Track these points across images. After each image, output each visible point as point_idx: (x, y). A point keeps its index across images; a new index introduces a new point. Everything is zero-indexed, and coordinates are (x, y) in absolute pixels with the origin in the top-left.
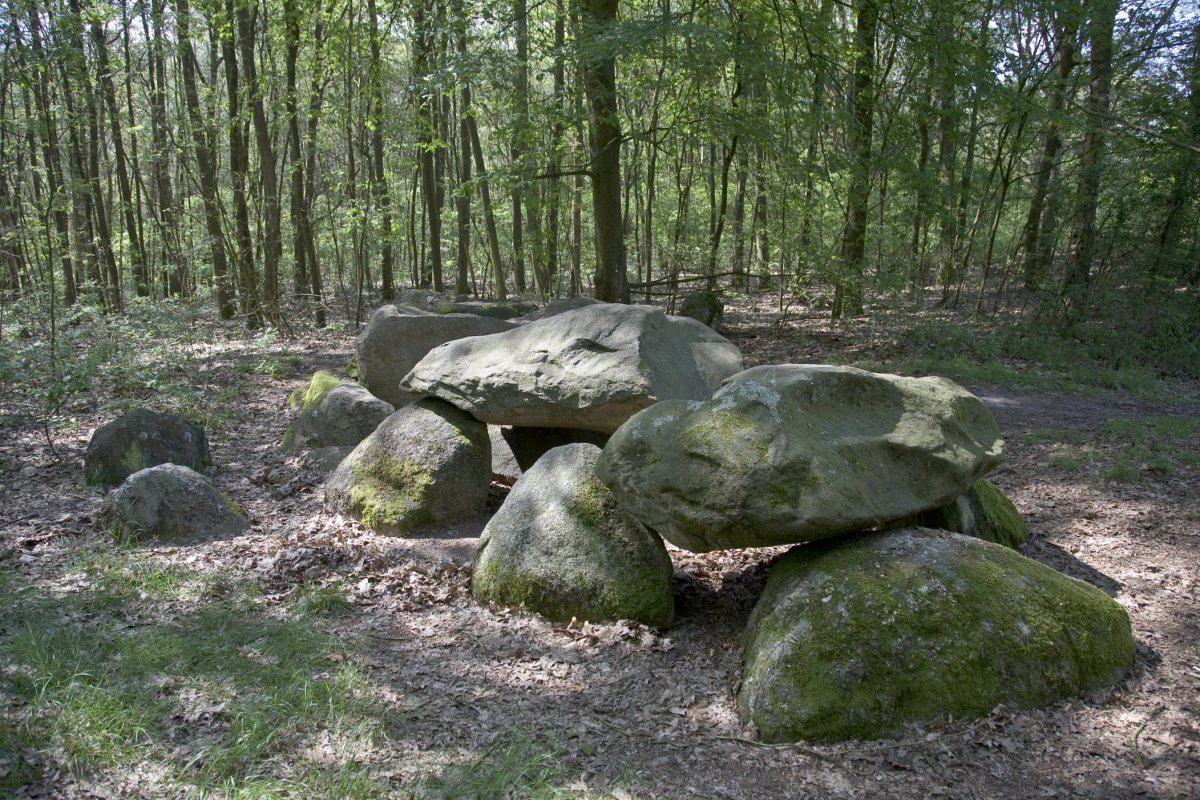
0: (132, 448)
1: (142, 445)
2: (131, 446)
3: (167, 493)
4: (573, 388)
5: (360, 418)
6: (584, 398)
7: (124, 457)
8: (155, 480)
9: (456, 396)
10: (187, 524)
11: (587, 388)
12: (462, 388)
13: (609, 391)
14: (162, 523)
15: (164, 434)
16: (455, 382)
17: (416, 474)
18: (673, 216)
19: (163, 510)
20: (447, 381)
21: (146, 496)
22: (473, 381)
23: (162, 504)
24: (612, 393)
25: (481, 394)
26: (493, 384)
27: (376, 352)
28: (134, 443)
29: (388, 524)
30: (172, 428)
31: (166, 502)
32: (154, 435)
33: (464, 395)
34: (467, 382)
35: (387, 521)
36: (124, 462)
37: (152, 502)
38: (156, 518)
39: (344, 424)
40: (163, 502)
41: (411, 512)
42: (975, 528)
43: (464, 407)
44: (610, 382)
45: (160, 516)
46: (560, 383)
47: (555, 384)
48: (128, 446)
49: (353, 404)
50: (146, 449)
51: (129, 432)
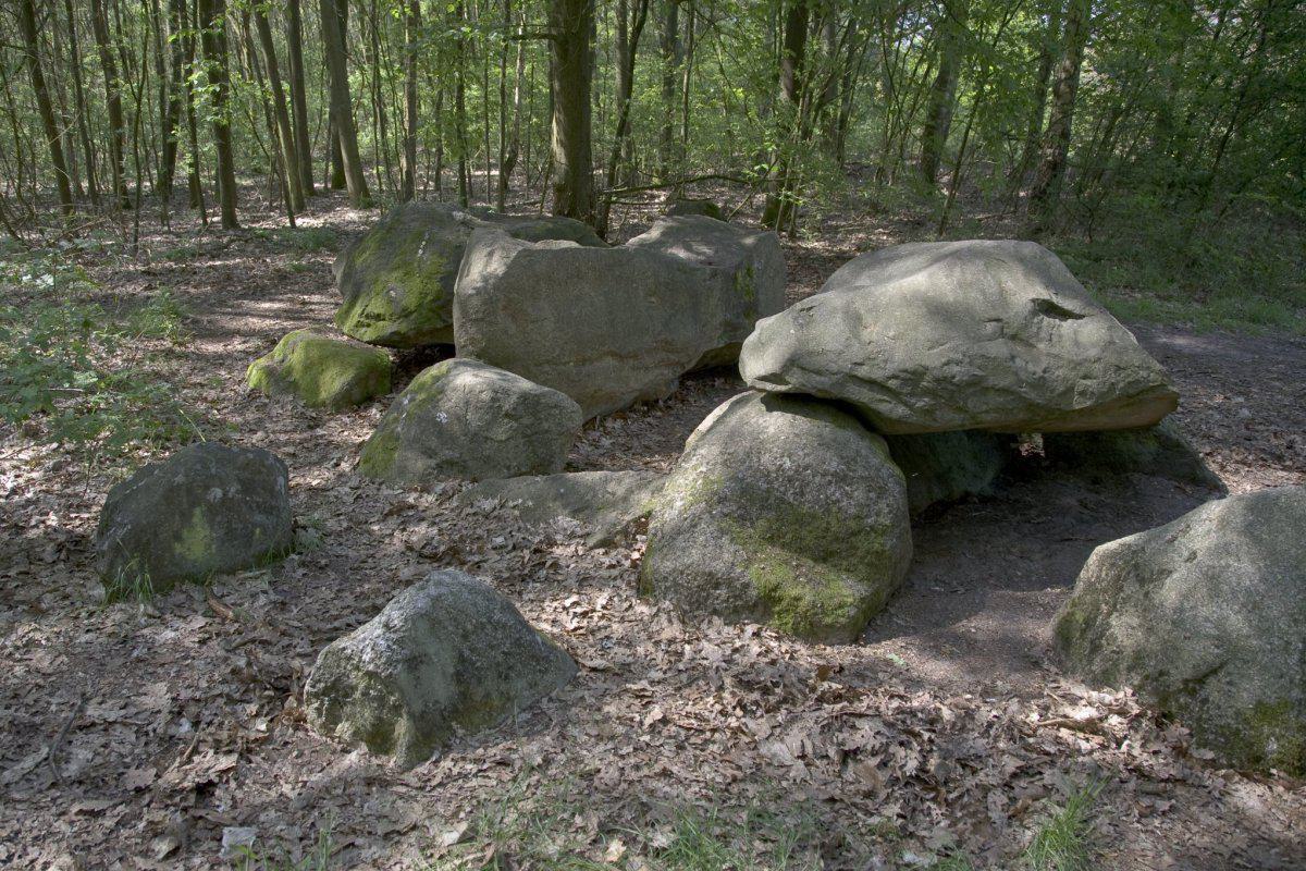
0: (195, 520)
1: (212, 511)
2: (192, 516)
3: (465, 637)
4: (1065, 379)
5: (526, 421)
6: (1082, 394)
7: (178, 537)
8: (442, 615)
9: (879, 397)
10: (503, 687)
11: (1085, 377)
12: (892, 383)
13: (1118, 382)
14: (464, 696)
15: (248, 487)
16: (878, 375)
17: (854, 534)
18: (100, 78)
19: (463, 674)
20: (863, 372)
21: (431, 651)
22: (914, 373)
23: (462, 659)
24: (1121, 385)
25: (927, 392)
26: (954, 377)
27: (505, 308)
28: (197, 511)
29: (830, 626)
30: (260, 472)
31: (467, 653)
32: (233, 490)
33: (895, 394)
34: (903, 375)
35: (828, 620)
36: (178, 548)
37: (443, 658)
38: (453, 688)
39: (501, 432)
40: (461, 655)
41: (862, 600)
42: (36, 367)
43: (894, 415)
44: (1119, 368)
45: (459, 682)
46: (1044, 372)
47: (1040, 373)
48: (186, 517)
49: (514, 398)
50: (219, 519)
51: (189, 491)
